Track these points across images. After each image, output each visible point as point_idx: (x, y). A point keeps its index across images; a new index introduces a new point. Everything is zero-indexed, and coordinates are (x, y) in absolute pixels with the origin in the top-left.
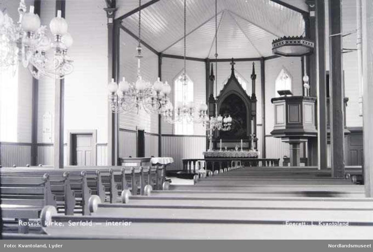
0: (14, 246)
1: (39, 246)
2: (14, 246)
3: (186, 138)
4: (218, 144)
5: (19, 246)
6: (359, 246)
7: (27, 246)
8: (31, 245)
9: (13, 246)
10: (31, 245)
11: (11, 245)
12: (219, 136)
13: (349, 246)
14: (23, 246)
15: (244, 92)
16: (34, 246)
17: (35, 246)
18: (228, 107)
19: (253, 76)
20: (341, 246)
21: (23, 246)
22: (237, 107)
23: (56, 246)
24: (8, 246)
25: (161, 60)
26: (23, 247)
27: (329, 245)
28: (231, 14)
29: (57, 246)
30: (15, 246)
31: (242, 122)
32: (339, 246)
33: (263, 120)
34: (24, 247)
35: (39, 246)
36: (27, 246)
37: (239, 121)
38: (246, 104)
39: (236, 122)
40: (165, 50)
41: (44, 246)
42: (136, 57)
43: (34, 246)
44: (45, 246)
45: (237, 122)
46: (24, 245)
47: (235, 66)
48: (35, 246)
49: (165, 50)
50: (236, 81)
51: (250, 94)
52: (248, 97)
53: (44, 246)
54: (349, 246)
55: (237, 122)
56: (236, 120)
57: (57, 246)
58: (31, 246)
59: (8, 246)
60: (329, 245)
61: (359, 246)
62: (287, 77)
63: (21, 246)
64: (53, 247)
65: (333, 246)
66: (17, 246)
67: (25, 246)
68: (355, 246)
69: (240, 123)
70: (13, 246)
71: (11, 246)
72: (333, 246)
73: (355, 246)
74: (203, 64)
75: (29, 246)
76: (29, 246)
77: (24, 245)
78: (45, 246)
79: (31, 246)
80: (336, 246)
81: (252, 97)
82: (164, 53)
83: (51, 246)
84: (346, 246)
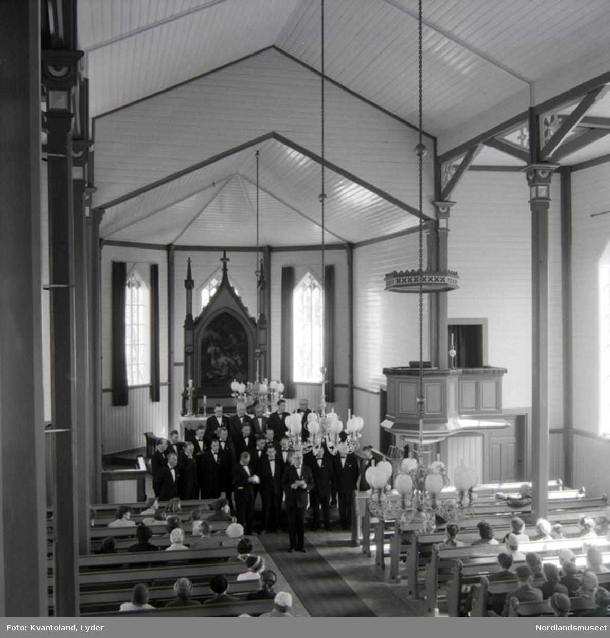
0: (23, 628)
1: (64, 628)
2: (23, 628)
3: (138, 390)
4: (199, 401)
5: (32, 628)
6: (587, 628)
7: (44, 628)
8: (51, 626)
9: (22, 628)
10: (18, 626)
11: (18, 626)
12: (200, 387)
13: (570, 628)
14: (38, 627)
15: (245, 310)
16: (56, 628)
17: (59, 628)
18: (216, 336)
19: (262, 283)
20: (558, 628)
21: (38, 627)
22: (231, 336)
23: (93, 628)
24: (14, 628)
25: (173, 256)
26: (38, 630)
27: (537, 626)
28: (224, 181)
29: (95, 628)
30: (25, 628)
31: (240, 362)
32: (553, 628)
33: (172, 350)
34: (40, 629)
35: (64, 628)
36: (44, 628)
37: (236, 361)
38: (248, 332)
39: (229, 363)
40: (176, 240)
41: (73, 628)
42: (189, 259)
43: (56, 628)
44: (74, 628)
45: (232, 361)
46: (40, 627)
47: (228, 264)
48: (59, 628)
49: (176, 240)
50: (231, 290)
51: (253, 313)
52: (252, 320)
53: (73, 628)
54: (570, 628)
55: (232, 361)
56: (229, 359)
57: (95, 628)
58: (51, 628)
59: (14, 628)
60: (537, 626)
61: (587, 628)
62: (315, 286)
63: (35, 628)
64: (88, 630)
65: (544, 628)
66: (29, 628)
67: (41, 628)
68: (579, 628)
69: (237, 364)
70: (22, 628)
71: (19, 628)
72: (544, 628)
73: (579, 628)
74: (164, 253)
75: (48, 628)
76: (48, 628)
77: (40, 627)
78: (74, 628)
79: (51, 628)
80: (550, 628)
81: (259, 321)
82: (176, 244)
83: (84, 628)
84: (565, 628)
